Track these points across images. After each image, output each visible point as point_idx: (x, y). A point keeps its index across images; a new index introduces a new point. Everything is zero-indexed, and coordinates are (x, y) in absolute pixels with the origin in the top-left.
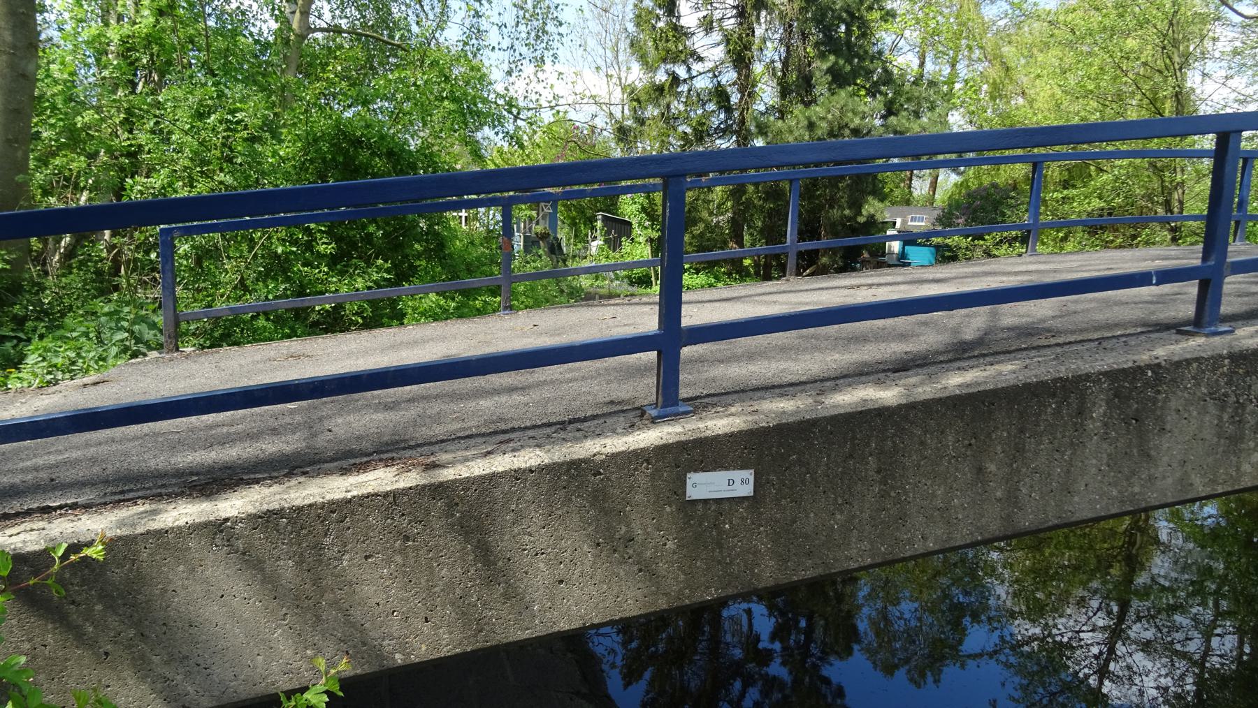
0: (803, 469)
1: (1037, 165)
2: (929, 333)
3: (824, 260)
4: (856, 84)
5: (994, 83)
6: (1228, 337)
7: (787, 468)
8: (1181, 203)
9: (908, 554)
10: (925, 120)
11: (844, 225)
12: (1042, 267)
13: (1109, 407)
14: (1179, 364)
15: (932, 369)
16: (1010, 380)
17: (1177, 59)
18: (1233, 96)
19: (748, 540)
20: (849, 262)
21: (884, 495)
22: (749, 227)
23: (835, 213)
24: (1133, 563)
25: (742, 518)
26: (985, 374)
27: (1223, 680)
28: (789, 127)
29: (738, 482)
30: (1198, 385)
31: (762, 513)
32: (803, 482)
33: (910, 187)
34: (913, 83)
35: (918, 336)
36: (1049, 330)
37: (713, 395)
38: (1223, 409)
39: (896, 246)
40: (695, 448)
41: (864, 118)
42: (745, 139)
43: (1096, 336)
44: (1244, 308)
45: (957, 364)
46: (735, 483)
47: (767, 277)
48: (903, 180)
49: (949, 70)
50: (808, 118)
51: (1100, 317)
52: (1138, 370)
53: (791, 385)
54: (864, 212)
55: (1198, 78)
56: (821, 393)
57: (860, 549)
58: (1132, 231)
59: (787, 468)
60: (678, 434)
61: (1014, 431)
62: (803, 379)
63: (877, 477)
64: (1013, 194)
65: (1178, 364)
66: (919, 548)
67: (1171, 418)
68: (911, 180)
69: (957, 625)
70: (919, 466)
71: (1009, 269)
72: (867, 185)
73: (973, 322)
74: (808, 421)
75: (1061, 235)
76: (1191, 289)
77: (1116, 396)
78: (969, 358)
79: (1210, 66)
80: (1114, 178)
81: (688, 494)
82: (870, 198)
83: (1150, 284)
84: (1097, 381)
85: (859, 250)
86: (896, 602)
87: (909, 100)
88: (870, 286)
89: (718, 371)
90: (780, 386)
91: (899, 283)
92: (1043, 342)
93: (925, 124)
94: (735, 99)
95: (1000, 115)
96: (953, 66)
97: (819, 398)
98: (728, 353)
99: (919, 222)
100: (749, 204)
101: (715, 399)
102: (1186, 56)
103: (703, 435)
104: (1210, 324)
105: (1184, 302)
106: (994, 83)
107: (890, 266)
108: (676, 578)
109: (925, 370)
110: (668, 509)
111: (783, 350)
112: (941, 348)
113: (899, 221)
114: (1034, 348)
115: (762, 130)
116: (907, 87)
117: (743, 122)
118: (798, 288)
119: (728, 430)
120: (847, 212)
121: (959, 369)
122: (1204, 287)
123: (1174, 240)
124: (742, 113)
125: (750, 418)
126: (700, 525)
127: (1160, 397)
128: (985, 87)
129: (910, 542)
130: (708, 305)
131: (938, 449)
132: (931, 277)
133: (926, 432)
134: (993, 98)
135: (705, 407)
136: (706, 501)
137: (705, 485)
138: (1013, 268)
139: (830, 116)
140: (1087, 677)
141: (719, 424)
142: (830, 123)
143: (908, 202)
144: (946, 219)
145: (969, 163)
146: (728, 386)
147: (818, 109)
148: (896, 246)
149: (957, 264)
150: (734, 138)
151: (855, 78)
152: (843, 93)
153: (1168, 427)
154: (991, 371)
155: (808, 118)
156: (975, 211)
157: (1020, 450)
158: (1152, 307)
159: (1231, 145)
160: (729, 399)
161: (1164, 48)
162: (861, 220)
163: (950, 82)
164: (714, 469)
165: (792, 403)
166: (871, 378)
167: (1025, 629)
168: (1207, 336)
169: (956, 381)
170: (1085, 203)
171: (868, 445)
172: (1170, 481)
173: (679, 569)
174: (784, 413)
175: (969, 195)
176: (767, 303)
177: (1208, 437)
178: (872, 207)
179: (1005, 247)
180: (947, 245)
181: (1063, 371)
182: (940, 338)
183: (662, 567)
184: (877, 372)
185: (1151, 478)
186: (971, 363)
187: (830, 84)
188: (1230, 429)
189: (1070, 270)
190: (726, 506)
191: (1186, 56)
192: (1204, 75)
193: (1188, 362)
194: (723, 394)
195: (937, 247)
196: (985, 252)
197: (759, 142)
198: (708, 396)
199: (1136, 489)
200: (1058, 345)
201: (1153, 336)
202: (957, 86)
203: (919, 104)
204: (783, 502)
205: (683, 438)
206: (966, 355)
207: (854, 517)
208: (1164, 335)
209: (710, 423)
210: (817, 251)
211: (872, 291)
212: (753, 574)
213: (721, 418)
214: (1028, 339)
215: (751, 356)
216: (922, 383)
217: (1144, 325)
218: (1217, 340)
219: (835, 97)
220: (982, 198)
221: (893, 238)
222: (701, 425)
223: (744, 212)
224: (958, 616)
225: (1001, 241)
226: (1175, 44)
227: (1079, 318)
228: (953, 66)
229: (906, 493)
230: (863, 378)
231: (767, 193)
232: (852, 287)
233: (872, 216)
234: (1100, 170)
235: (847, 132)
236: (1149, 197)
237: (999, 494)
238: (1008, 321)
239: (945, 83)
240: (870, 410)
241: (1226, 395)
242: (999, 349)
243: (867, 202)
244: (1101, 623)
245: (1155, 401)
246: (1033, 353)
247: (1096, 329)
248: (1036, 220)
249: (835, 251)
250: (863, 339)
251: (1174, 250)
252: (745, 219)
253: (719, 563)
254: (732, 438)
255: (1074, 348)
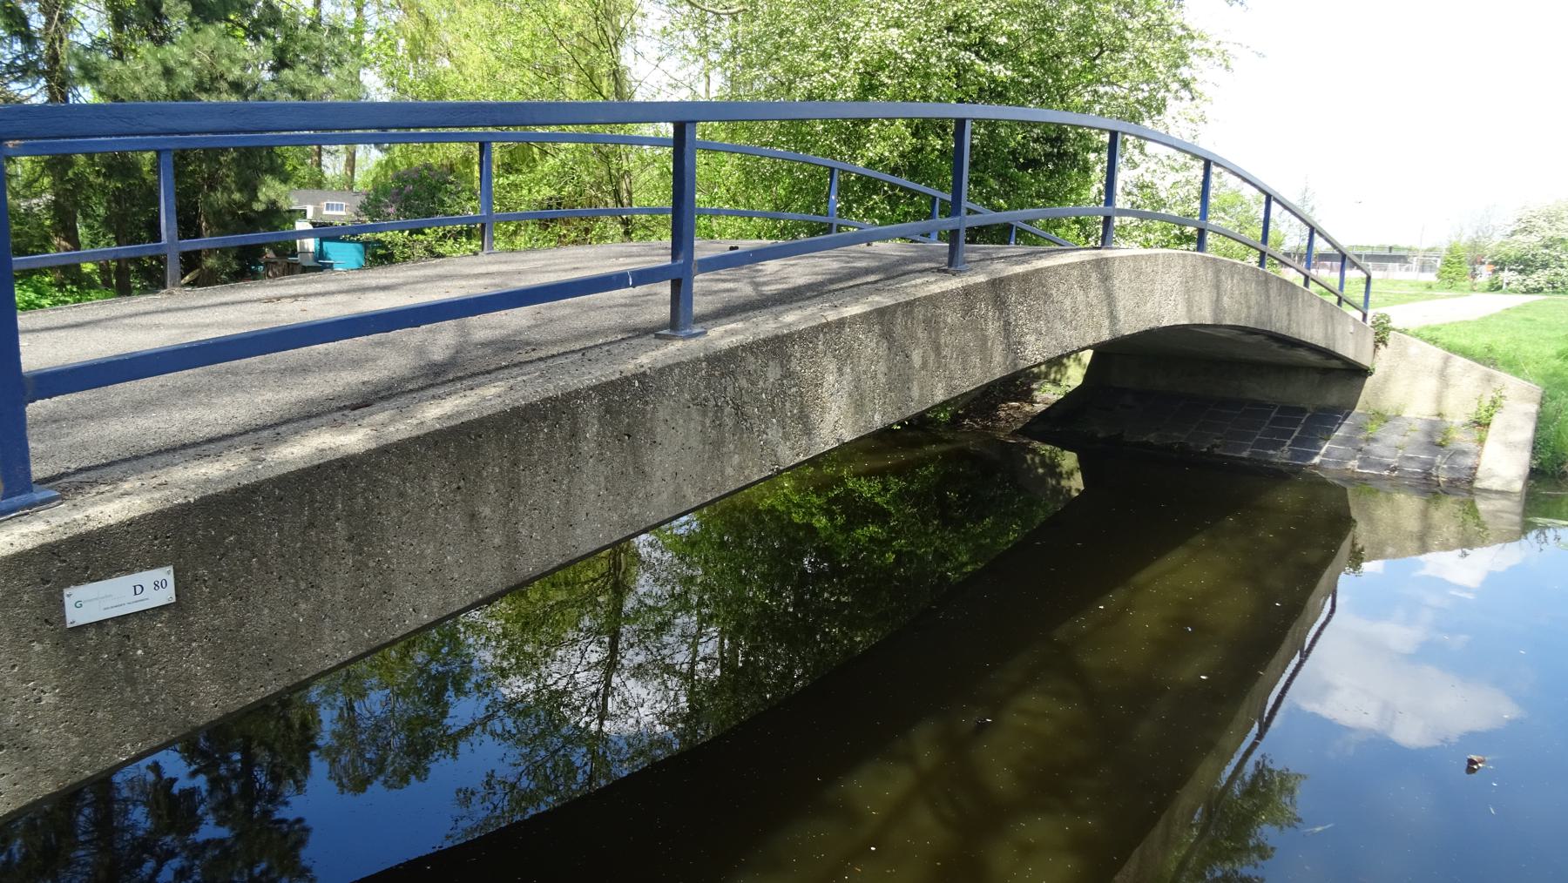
0: (247, 553)
1: (484, 147)
2: (390, 357)
3: (211, 262)
4: (229, 20)
5: (413, 38)
6: (702, 339)
7: (223, 555)
8: (630, 193)
9: (398, 634)
10: (331, 78)
11: (234, 214)
12: (504, 268)
13: (602, 425)
14: (663, 371)
15: (402, 400)
16: (496, 406)
17: (611, 33)
18: (666, 79)
19: (176, 664)
20: (246, 266)
21: (359, 567)
22: (86, 216)
23: (219, 197)
24: (620, 589)
25: (163, 636)
26: (465, 401)
27: (714, 690)
28: (134, 72)
29: (149, 587)
30: (681, 391)
31: (192, 624)
32: (248, 571)
33: (319, 164)
34: (310, 27)
35: (374, 360)
36: (528, 344)
37: (88, 469)
38: (704, 414)
39: (311, 244)
40: (72, 550)
41: (244, 69)
42: (62, 84)
43: (578, 346)
44: (711, 308)
45: (430, 392)
46: (151, 588)
47: (124, 290)
48: (310, 156)
49: (354, 15)
50: (163, 62)
51: (579, 324)
52: (627, 381)
53: (211, 441)
54: (261, 196)
55: (631, 55)
56: (258, 447)
57: (337, 641)
58: (584, 224)
59: (223, 555)
60: (42, 534)
61: (506, 465)
62: (228, 430)
63: (350, 546)
64: (451, 178)
65: (661, 371)
66: (411, 623)
67: (660, 429)
68: (320, 155)
69: (437, 699)
70: (400, 524)
71: (467, 271)
72: (258, 162)
73: (441, 339)
74: (246, 487)
75: (511, 228)
76: (664, 289)
77: (607, 411)
78: (443, 383)
79: (642, 45)
80: (555, 166)
81: (69, 618)
82: (268, 178)
83: (627, 286)
84: (587, 398)
85: (258, 250)
86: (362, 695)
87: (306, 49)
88: (296, 297)
89: (88, 432)
90: (195, 444)
91: (333, 293)
92: (524, 357)
93: (328, 86)
94: (37, 22)
95: (426, 79)
96: (359, 11)
97: (256, 454)
98: (99, 406)
99: (340, 212)
100: (80, 182)
101: (93, 475)
102: (620, 32)
103: (83, 530)
104: (686, 326)
105: (656, 303)
106: (413, 38)
107: (305, 270)
108: (65, 745)
109: (393, 403)
110: (37, 647)
111: (187, 392)
112: (407, 373)
113: (310, 210)
114: (515, 365)
115: (90, 74)
116: (302, 32)
117: (54, 59)
118: (188, 303)
119: (124, 516)
120: (237, 196)
121: (434, 397)
122: (677, 285)
123: (627, 233)
124: (52, 46)
125: (157, 495)
126: (95, 660)
127: (649, 408)
128: (402, 42)
129: (400, 618)
130: (46, 335)
131: (422, 499)
132: (374, 283)
133: (404, 480)
134: (414, 58)
135: (79, 488)
136: (100, 624)
137: (88, 603)
138: (464, 272)
139: (195, 62)
140: (588, 724)
141: (109, 509)
142: (198, 72)
143: (319, 185)
144: (372, 206)
145: (395, 140)
146: (113, 453)
147: (175, 49)
148: (311, 244)
149: (395, 268)
150: (43, 82)
151: (227, 11)
152: (211, 31)
153: (658, 440)
154: (472, 398)
155: (163, 62)
156: (408, 198)
157: (515, 485)
158: (628, 310)
159: (687, 136)
160: (117, 471)
161: (597, 19)
162: (258, 207)
163: (358, 32)
164: (108, 576)
165: (217, 465)
166: (324, 419)
167: (518, 687)
168: (683, 339)
169: (435, 412)
170: (535, 190)
171: (332, 507)
172: (665, 496)
173: (68, 729)
174: (208, 481)
175: (398, 178)
176: (149, 327)
177: (694, 444)
178: (271, 190)
179: (450, 242)
180: (379, 241)
181: (551, 390)
182: (403, 361)
183: (38, 733)
184: (330, 412)
185: (648, 496)
186: (446, 389)
187: (190, 16)
188: (713, 434)
189: (535, 271)
190: (135, 624)
191: (620, 32)
192: (637, 53)
193: (671, 368)
194: (104, 465)
195: (366, 244)
196: (426, 249)
197: (86, 95)
198: (79, 471)
199: (635, 511)
200: (540, 359)
201: (634, 342)
202: (368, 37)
203: (320, 55)
204: (222, 602)
205: (49, 539)
206: (439, 380)
207: (324, 602)
208: (644, 340)
209: (92, 511)
210: (198, 253)
211: (299, 304)
212: (188, 710)
213: (110, 501)
214: (507, 356)
215: (139, 407)
216: (392, 421)
217: (624, 330)
218: (693, 343)
219: (201, 36)
220: (414, 182)
221: (305, 234)
222: (79, 516)
223: (73, 193)
224: (440, 687)
225: (444, 236)
226: (608, 15)
227: (557, 326)
228: (359, 11)
229: (388, 559)
230: (313, 421)
231: (109, 167)
232: (270, 300)
233: (274, 203)
234: (544, 153)
235: (224, 85)
236: (598, 186)
237: (497, 541)
238: (480, 335)
239: (351, 32)
240: (330, 462)
241: (706, 399)
242: (476, 370)
243: (264, 183)
244: (594, 658)
245: (644, 413)
246: (515, 371)
247: (577, 338)
248: (490, 209)
249: (224, 251)
250: (304, 369)
251: (634, 246)
252: (76, 204)
253: (133, 706)
254: (132, 527)
255: (559, 361)
